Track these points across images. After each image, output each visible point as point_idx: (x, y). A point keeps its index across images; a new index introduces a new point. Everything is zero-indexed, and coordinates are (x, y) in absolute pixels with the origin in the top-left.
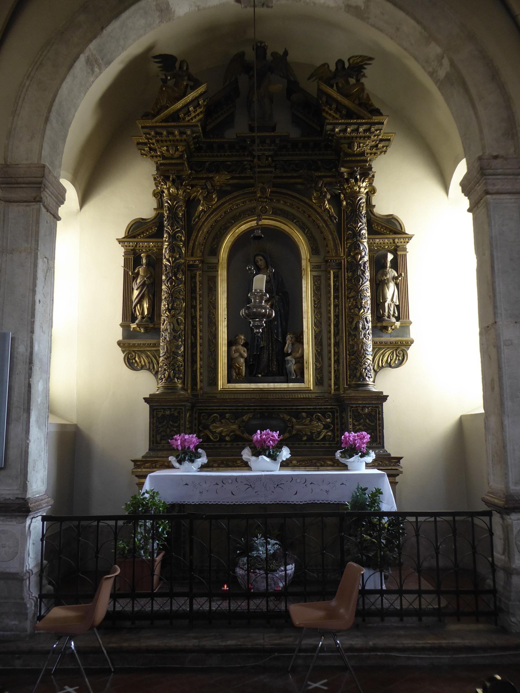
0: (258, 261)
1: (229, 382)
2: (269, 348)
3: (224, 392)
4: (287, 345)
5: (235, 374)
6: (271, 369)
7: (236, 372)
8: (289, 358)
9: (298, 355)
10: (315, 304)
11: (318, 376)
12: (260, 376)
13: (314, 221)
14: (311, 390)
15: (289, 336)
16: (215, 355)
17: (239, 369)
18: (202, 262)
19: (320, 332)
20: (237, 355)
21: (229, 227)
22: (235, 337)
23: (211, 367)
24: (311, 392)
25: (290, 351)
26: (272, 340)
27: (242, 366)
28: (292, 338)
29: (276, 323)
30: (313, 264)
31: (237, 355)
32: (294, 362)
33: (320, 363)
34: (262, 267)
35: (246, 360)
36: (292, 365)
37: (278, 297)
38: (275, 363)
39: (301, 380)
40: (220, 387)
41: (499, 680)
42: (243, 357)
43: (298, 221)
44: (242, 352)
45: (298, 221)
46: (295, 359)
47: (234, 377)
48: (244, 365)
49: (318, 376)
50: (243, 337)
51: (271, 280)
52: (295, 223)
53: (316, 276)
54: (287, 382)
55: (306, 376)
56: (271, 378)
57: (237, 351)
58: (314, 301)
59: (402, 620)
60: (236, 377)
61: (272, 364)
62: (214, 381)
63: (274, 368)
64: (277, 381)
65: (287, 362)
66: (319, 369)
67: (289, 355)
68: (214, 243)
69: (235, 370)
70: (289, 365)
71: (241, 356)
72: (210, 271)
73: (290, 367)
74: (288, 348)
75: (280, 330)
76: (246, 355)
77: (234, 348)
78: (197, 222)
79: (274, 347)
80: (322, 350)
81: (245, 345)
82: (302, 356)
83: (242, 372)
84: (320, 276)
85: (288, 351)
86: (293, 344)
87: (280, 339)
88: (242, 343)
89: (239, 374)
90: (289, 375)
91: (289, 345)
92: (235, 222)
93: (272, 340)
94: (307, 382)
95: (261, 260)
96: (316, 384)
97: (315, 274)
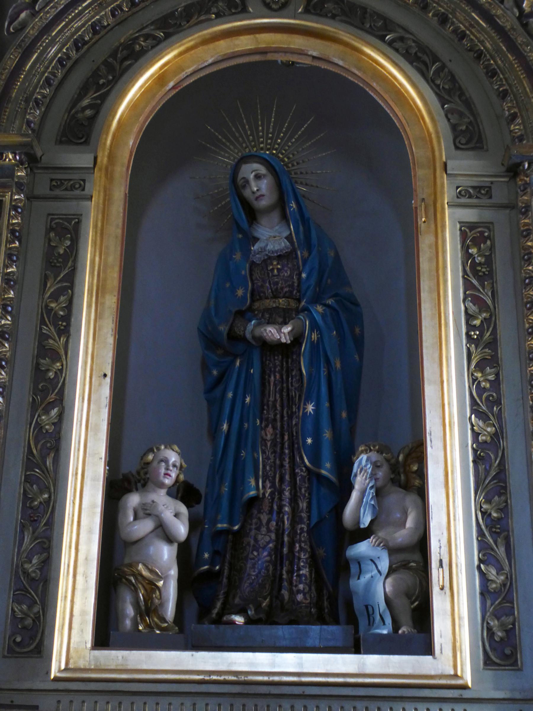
0: (247, 182)
1: (103, 639)
2: (281, 508)
3: (79, 687)
4: (355, 495)
5: (130, 611)
6: (285, 593)
7: (136, 604)
8: (363, 548)
9: (403, 535)
10: (470, 327)
11: (494, 623)
12: (239, 620)
13: (463, 36)
14: (464, 687)
15: (364, 457)
16: (50, 524)
17: (152, 587)
18: (31, 160)
19: (497, 436)
20: (145, 527)
21: (143, 52)
22: (146, 454)
23: (26, 573)
24: (466, 694)
25: (366, 521)
26: (293, 475)
27: (166, 578)
28: (376, 466)
29: (310, 408)
30: (460, 181)
31: (145, 527)
32: (384, 564)
33: (500, 570)
34: (264, 203)
35: (185, 555)
36: (375, 579)
37: (320, 308)
38: (304, 571)
39: (420, 638)
40: (57, 666)
41: (13, 291)
42: (169, 539)
43: (402, 39)
44: (168, 515)
45: (402, 39)
46: (393, 551)
47: (128, 623)
48: (174, 572)
49: (494, 623)
50: (173, 457)
51: (294, 251)
52: (390, 44)
53: (472, 226)
54: (356, 647)
55: (441, 625)
56: (283, 631)
57: (145, 511)
58: (469, 317)
59: (303, 692)
60: (135, 624)
61: (290, 572)
62: (33, 635)
63: (302, 594)
64: (310, 643)
65: (354, 569)
66: (496, 593)
67: (362, 534)
68: (86, 102)
69: (135, 591)
70: (365, 578)
71: (163, 532)
72: (56, 198)
73: (369, 585)
74: (358, 508)
75: (327, 435)
76: (182, 530)
77: (134, 500)
78: (23, 26)
79: (303, 505)
80: (505, 509)
81: (185, 492)
82: (422, 544)
83: (162, 604)
84: (489, 225)
85: (358, 522)
86: (379, 493)
87: (327, 470)
88: (168, 481)
89: (149, 609)
90: (363, 623)
91: (363, 493)
92: (168, 36)
93: (293, 475)
94: (448, 652)
95: (258, 177)
96: (488, 662)
97: (470, 215)
